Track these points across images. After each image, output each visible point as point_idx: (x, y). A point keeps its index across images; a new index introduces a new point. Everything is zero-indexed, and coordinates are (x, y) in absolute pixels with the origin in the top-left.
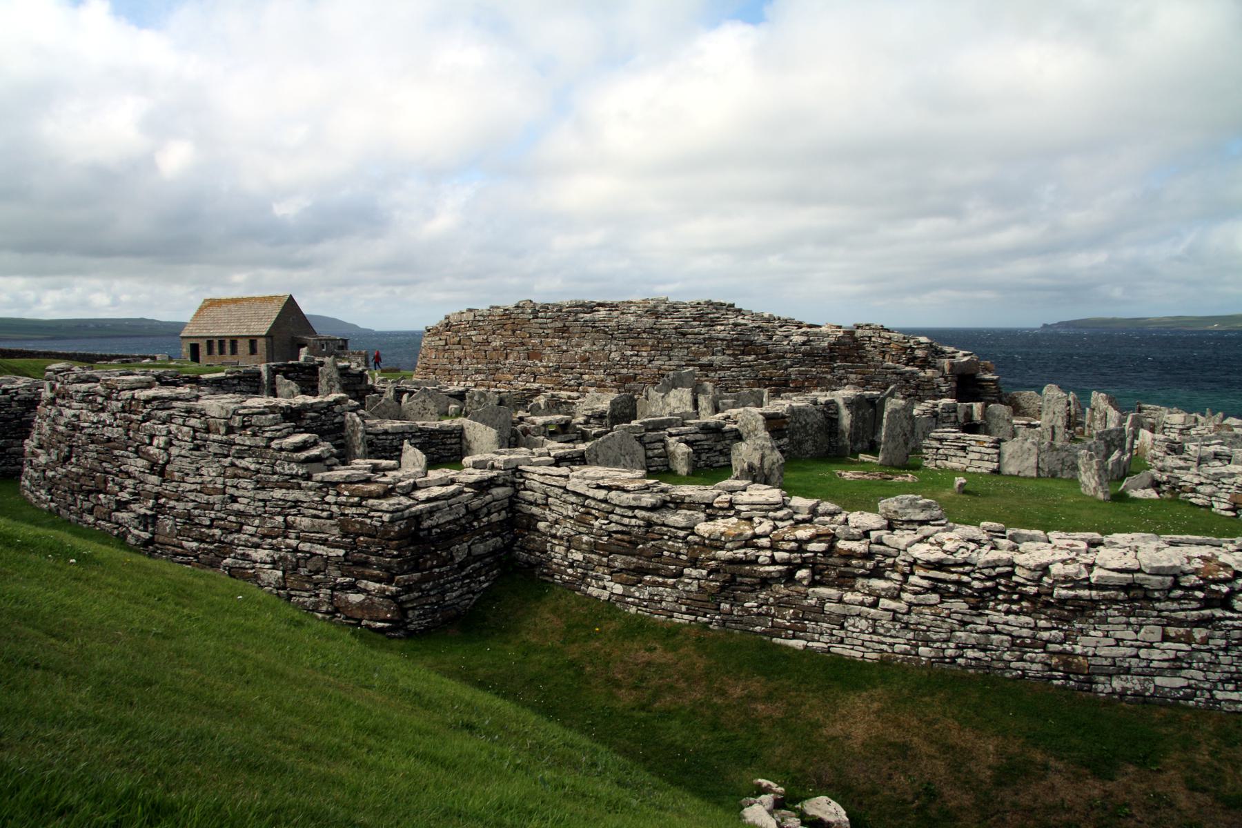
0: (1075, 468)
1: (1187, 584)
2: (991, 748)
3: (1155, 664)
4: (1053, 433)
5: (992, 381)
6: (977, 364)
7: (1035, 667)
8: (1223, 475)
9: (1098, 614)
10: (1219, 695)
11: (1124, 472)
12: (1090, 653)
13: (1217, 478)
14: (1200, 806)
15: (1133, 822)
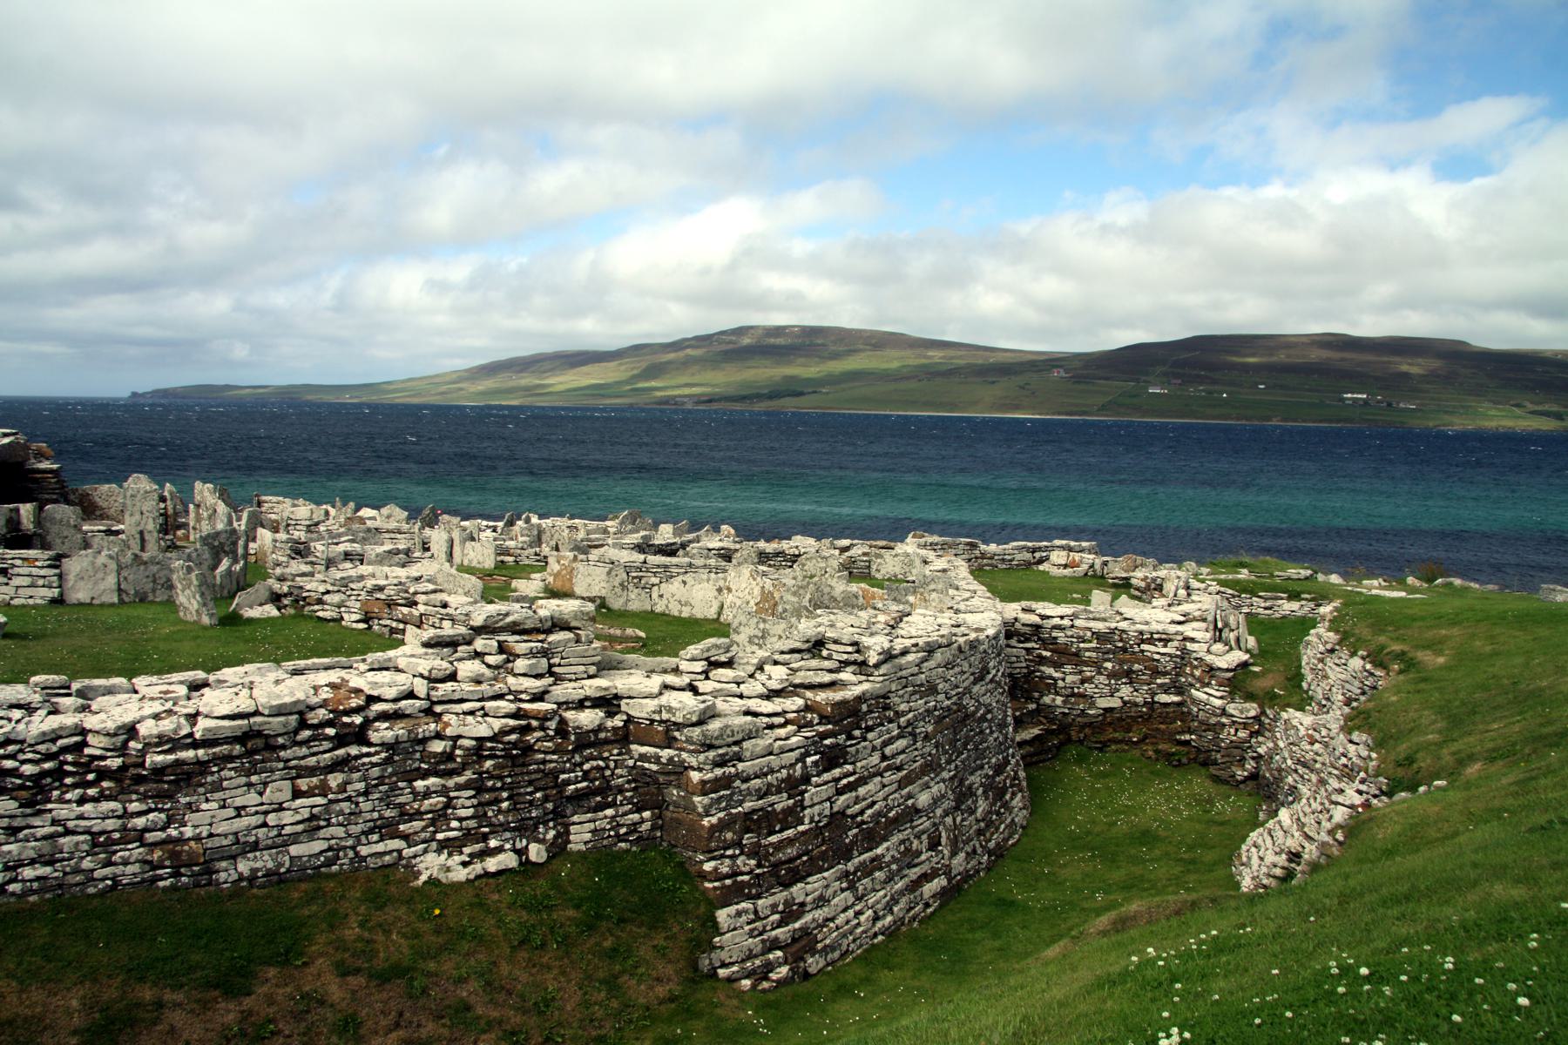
0: (171, 587)
1: (315, 721)
2: (75, 1003)
3: (288, 830)
4: (143, 540)
5: (51, 471)
6: (26, 447)
7: (130, 869)
8: (350, 579)
9: (209, 779)
10: (364, 851)
11: (240, 583)
12: (205, 834)
13: (345, 583)
14: (354, 992)
15: (281, 1040)
